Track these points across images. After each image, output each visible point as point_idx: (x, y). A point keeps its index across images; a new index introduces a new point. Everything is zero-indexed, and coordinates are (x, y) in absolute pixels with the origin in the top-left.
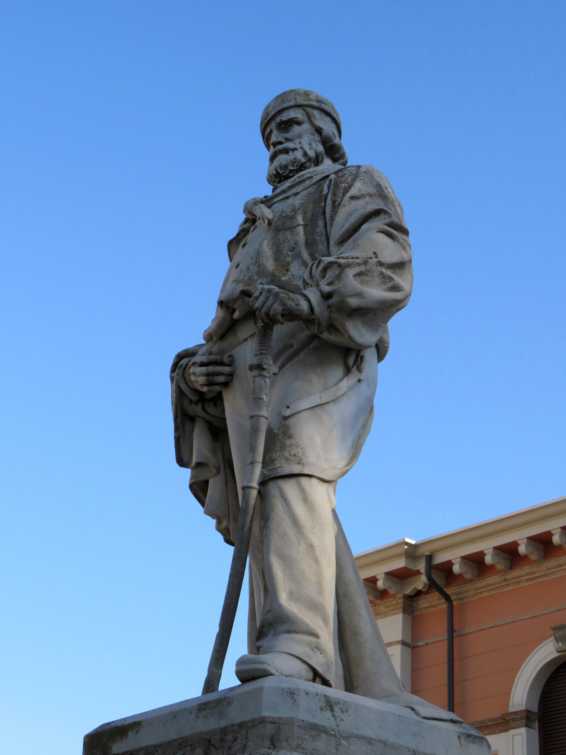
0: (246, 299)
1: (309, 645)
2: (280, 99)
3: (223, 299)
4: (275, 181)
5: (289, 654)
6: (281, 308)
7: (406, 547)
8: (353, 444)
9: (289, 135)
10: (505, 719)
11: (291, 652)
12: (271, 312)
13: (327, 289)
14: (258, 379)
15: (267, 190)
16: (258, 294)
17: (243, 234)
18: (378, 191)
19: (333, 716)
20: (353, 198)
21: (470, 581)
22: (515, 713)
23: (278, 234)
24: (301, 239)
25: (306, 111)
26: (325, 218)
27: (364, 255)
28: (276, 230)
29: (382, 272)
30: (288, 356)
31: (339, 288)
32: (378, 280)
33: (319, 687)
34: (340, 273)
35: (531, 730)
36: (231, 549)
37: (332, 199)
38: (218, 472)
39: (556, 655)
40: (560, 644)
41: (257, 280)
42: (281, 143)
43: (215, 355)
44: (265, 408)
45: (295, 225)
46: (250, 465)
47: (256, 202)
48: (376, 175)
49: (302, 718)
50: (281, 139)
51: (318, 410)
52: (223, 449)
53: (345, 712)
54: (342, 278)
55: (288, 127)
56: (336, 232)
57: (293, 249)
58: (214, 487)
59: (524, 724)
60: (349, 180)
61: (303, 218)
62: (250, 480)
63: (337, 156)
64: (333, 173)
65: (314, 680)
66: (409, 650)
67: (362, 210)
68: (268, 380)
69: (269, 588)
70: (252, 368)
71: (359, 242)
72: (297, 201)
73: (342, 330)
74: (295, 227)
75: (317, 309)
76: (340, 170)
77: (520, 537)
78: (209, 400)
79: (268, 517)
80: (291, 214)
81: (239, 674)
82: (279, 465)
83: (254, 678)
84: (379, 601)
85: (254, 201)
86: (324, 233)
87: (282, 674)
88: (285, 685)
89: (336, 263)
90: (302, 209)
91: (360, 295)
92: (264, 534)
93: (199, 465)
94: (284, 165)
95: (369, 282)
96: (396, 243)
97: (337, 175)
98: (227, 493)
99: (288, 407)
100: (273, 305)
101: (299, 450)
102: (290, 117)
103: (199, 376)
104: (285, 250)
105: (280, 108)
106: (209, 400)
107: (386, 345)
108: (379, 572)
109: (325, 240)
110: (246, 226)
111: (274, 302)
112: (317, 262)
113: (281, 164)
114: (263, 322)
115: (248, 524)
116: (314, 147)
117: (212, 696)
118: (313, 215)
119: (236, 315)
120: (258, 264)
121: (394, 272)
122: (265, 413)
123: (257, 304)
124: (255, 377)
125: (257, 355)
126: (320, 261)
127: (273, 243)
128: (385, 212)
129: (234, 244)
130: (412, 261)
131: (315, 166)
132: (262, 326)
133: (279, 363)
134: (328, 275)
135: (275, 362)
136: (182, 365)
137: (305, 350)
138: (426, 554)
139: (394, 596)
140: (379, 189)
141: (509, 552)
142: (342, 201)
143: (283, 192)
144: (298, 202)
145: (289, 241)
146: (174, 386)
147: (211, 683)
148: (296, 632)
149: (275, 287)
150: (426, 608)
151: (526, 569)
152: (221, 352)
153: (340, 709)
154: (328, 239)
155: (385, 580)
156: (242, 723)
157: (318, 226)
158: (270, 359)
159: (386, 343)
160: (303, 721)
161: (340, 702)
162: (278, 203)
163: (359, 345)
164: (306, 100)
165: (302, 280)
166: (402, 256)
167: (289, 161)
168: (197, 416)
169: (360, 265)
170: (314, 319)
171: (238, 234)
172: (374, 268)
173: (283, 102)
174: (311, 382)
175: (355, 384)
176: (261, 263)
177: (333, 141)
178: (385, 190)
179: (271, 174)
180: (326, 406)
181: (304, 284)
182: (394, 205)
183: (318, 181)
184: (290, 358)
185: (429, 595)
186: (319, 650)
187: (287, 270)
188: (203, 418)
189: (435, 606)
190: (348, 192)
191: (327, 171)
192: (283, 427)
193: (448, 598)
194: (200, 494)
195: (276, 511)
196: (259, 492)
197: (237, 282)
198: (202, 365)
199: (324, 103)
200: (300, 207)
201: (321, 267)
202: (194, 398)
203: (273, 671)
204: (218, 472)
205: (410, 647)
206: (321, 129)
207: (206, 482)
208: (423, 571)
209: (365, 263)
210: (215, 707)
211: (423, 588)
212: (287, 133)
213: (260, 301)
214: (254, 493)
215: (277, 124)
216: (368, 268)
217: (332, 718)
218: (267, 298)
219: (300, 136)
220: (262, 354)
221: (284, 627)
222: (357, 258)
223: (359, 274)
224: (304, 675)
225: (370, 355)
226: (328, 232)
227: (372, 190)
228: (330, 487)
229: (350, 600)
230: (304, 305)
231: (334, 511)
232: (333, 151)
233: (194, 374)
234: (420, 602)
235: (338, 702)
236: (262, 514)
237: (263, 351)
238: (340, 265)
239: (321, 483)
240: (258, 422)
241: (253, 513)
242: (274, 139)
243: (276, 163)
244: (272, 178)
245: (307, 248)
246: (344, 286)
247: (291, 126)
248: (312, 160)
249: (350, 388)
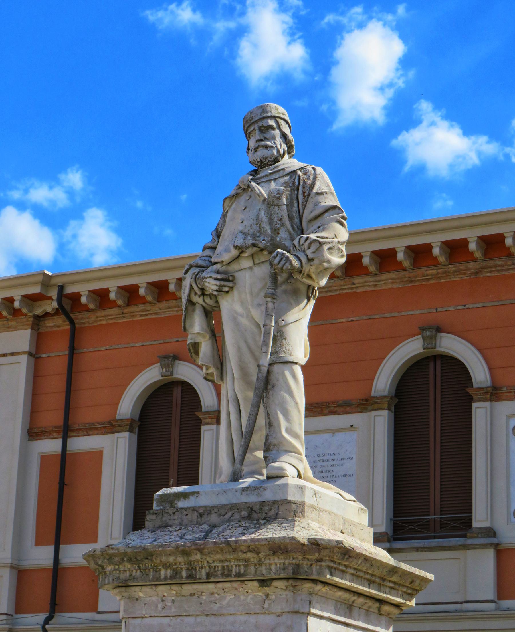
10: (112, 424)
21: (92, 310)
22: (122, 420)
23: (269, 208)
25: (277, 121)
28: (268, 204)
32: (337, 252)
35: (132, 434)
39: (160, 378)
40: (164, 370)
57: (280, 220)
59: (128, 430)
66: (33, 359)
77: (142, 281)
84: (11, 317)
104: (276, 219)
105: (262, 117)
111: (286, 262)
139: (26, 315)
141: (130, 293)
150: (50, 327)
151: (142, 307)
156: (275, 501)
187: (278, 233)
189: (59, 327)
193: (72, 322)
202: (199, 293)
208: (55, 297)
210: (254, 490)
218: (282, 259)
223: (330, 249)
234: (46, 322)
238: (320, 243)
247: (268, 129)
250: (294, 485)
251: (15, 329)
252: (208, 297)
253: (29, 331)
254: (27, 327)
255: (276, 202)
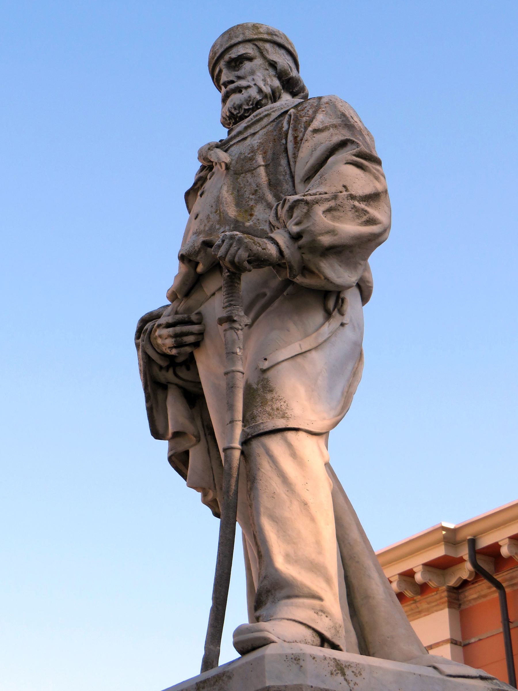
0: (209, 249)
1: (313, 609)
2: (227, 36)
3: (183, 252)
4: (230, 123)
5: (291, 620)
6: (247, 254)
7: (444, 532)
8: (343, 393)
9: (240, 73)
11: (294, 618)
12: (236, 259)
13: (295, 229)
14: (228, 333)
15: (223, 134)
16: (220, 242)
17: (199, 183)
18: (343, 121)
19: (346, 680)
20: (316, 131)
23: (237, 178)
24: (263, 180)
25: (256, 45)
26: (288, 156)
27: (333, 190)
28: (235, 174)
29: (354, 206)
30: (261, 306)
31: (308, 227)
32: (350, 214)
33: (327, 651)
34: (308, 211)
36: (219, 520)
37: (293, 135)
38: (199, 441)
41: (219, 229)
42: (232, 82)
43: (181, 314)
44: (240, 362)
45: (255, 167)
46: (229, 425)
47: (211, 147)
48: (339, 105)
49: (311, 684)
50: (231, 78)
51: (299, 359)
52: (202, 418)
53: (358, 675)
54: (311, 216)
55: (239, 65)
56: (301, 169)
57: (255, 192)
58: (196, 457)
60: (311, 112)
61: (263, 158)
62: (231, 440)
63: (296, 89)
64: (292, 108)
65: (322, 645)
66: (459, 649)
67: (327, 142)
68: (240, 332)
69: (263, 553)
70: (221, 321)
71: (326, 176)
72: (255, 141)
73: (316, 271)
74: (255, 169)
75: (287, 252)
76: (300, 104)
78: (181, 364)
79: (254, 478)
80: (249, 156)
81: (236, 645)
82: (261, 421)
83: (254, 649)
84: (419, 597)
85: (208, 147)
86: (288, 172)
87: (285, 641)
88: (289, 651)
89: (302, 200)
90: (261, 148)
91: (332, 232)
92: (252, 496)
93: (177, 435)
94: (238, 105)
95: (341, 217)
96: (367, 174)
97: (297, 110)
98: (211, 462)
99: (266, 359)
100: (237, 251)
101: (282, 403)
102: (239, 54)
103: (166, 339)
104: (247, 195)
105: (228, 45)
106: (181, 364)
107: (370, 285)
108: (416, 564)
109: (290, 179)
110: (202, 174)
111: (239, 249)
112: (281, 202)
113: (234, 104)
114: (229, 271)
115: (233, 487)
116: (269, 83)
117: (212, 673)
118: (274, 154)
119: (200, 268)
120: (218, 212)
121: (368, 205)
122: (241, 369)
123: (221, 252)
124: (225, 330)
125: (226, 307)
126: (285, 200)
127: (234, 189)
128: (352, 142)
129: (191, 195)
130: (389, 191)
131: (272, 103)
132: (228, 276)
133: (252, 315)
134: (295, 215)
135: (247, 313)
136: (147, 329)
137: (280, 298)
138: (469, 538)
140: (344, 119)
142: (304, 135)
143: (240, 133)
144: (256, 142)
145: (250, 184)
146: (140, 353)
147: (210, 659)
148: (297, 596)
149: (238, 233)
150: (475, 599)
152: (188, 310)
153: (353, 672)
154: (293, 177)
155: (423, 573)
157: (281, 165)
158: (240, 310)
159: (368, 282)
160: (312, 687)
161: (352, 665)
162: (235, 146)
163: (338, 286)
164: (255, 34)
165: (267, 224)
166: (375, 187)
167: (243, 100)
168: (169, 383)
169: (329, 201)
170: (285, 263)
171: (195, 184)
172: (346, 202)
173: (230, 38)
174: (288, 331)
175: (338, 329)
176: (221, 210)
177: (289, 74)
178: (351, 120)
179: (225, 116)
180: (308, 354)
181: (270, 227)
182: (362, 135)
183: (276, 118)
184: (264, 308)
185: (477, 585)
186: (324, 613)
188: (176, 385)
189: (485, 596)
190: (310, 125)
191: (286, 106)
192: (262, 380)
193: (498, 586)
194: (182, 467)
195: (263, 470)
196: (242, 453)
197: (197, 233)
198: (168, 326)
199: (276, 35)
200: (259, 147)
201: (286, 207)
203: (273, 637)
204: (199, 441)
205: (460, 645)
206: (276, 63)
207: (187, 453)
208: (466, 557)
209: (335, 197)
211: (469, 577)
212: (238, 70)
213: (223, 249)
214: (237, 454)
215: (227, 61)
216: (338, 202)
217: (344, 683)
218: (231, 245)
219: (252, 73)
220: (230, 305)
221: (284, 592)
222: (326, 193)
223: (329, 210)
224: (310, 641)
225: (352, 297)
226: (293, 170)
227: (336, 121)
228: (321, 441)
229: (358, 562)
230: (272, 250)
231: (327, 465)
232: (291, 85)
233: (160, 336)
234: (467, 594)
235: (349, 665)
236: (248, 476)
237: (232, 303)
238: (307, 203)
239: (310, 436)
240: (233, 377)
241: (238, 475)
242: (224, 78)
243: (229, 103)
244: (226, 120)
245: (270, 190)
246: (314, 224)
247: (241, 63)
248: (269, 96)
249: (333, 333)
250: (280, 655)
251: (428, 611)
252: (184, 368)
253: (446, 611)
254: (441, 607)
255: (247, 166)
